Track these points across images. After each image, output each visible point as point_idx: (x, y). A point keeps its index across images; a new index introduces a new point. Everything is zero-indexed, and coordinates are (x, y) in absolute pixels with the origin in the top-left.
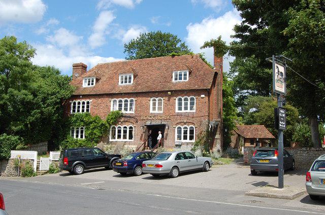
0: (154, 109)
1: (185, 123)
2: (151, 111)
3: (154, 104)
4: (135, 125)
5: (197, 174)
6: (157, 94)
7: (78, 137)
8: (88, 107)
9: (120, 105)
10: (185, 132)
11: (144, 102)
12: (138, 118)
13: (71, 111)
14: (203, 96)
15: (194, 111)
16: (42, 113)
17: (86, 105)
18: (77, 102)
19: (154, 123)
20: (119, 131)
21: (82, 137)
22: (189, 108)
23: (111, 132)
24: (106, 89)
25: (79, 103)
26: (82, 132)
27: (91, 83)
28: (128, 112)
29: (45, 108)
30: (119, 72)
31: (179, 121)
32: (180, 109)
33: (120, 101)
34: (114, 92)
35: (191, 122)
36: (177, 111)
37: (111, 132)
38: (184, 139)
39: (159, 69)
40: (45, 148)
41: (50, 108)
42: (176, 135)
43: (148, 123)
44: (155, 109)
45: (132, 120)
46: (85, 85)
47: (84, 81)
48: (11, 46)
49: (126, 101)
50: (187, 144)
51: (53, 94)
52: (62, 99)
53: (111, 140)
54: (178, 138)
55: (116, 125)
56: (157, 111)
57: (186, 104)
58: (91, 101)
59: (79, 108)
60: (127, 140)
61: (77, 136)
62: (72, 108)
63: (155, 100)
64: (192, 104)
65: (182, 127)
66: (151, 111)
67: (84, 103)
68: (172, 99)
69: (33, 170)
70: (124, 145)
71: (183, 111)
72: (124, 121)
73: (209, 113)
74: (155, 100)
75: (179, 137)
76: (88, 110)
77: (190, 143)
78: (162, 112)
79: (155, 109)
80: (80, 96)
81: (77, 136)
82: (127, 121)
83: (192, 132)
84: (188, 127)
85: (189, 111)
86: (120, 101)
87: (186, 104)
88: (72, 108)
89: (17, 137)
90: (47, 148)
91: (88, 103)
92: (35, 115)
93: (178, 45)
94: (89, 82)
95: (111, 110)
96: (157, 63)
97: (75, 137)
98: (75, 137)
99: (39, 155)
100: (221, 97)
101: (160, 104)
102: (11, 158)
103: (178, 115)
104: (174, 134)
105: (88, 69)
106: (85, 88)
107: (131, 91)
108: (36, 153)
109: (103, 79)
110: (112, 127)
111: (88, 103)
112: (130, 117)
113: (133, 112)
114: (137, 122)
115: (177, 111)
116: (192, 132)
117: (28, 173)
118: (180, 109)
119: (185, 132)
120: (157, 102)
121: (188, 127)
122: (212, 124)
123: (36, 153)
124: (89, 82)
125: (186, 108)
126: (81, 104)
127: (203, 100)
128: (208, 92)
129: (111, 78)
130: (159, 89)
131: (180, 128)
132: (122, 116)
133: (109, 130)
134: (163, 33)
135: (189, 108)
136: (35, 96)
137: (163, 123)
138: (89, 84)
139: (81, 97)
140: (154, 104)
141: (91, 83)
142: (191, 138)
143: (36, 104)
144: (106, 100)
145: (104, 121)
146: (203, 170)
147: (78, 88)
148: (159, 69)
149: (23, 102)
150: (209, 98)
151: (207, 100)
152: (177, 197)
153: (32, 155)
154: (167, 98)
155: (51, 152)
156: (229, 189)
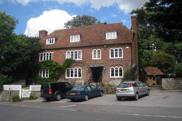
0: (95, 57)
1: (116, 66)
2: (93, 58)
3: (95, 54)
4: (82, 68)
5: (94, 99)
6: (97, 47)
7: (44, 75)
8: (50, 57)
9: (72, 55)
10: (117, 71)
11: (88, 53)
12: (84, 63)
13: (40, 60)
14: (127, 47)
15: (122, 57)
16: (23, 60)
17: (49, 56)
18: (43, 54)
19: (95, 66)
20: (72, 72)
21: (47, 76)
22: (114, 56)
23: (66, 71)
24: (63, 45)
25: (45, 55)
26: (47, 73)
27: (52, 42)
28: (78, 59)
29: (25, 57)
30: (69, 34)
31: (112, 64)
32: (112, 56)
33: (72, 52)
34: (67, 46)
35: (120, 64)
36: (110, 58)
37: (66, 71)
38: (116, 76)
39: (96, 32)
40: (24, 83)
41: (27, 57)
42: (110, 73)
43: (92, 66)
44: (96, 56)
45: (80, 64)
46: (48, 43)
47: (47, 40)
48: (2, 17)
49: (76, 52)
50: (118, 79)
51: (29, 48)
52: (34, 52)
53: (66, 78)
54: (120, 75)
55: (70, 68)
56: (97, 58)
57: (116, 53)
58: (53, 53)
59: (45, 57)
60: (78, 77)
61: (44, 75)
62: (40, 58)
63: (95, 51)
64: (120, 53)
65: (114, 68)
66: (93, 58)
67: (48, 54)
68: (108, 49)
69: (19, 97)
70: (76, 80)
71: (115, 57)
72: (75, 65)
73: (132, 59)
74: (68, 52)
75: (113, 75)
76: (50, 59)
77: (120, 78)
78: (100, 59)
79: (96, 56)
80: (45, 49)
81: (44, 75)
82: (77, 65)
83: (121, 71)
84: (119, 68)
85: (118, 57)
86: (72, 52)
87: (116, 53)
88: (40, 58)
89: (7, 76)
90: (25, 83)
91: (51, 54)
92: (15, 64)
93: (97, 22)
94: (51, 41)
95: (66, 58)
96: (94, 28)
97: (42, 76)
98: (42, 76)
99: (23, 87)
100: (137, 49)
101: (99, 53)
102: (4, 90)
103: (111, 60)
104: (109, 73)
105: (48, 34)
106: (48, 45)
107: (79, 46)
108: (20, 86)
109: (60, 39)
110: (67, 69)
111: (51, 54)
112: (79, 62)
113: (81, 59)
114: (84, 65)
115: (110, 58)
116: (121, 71)
117: (16, 98)
118: (112, 56)
119: (117, 71)
120: (97, 52)
121: (119, 68)
122: (134, 66)
123: (20, 86)
124: (51, 41)
125: (116, 56)
126: (46, 55)
127: (128, 50)
128: (130, 44)
129: (64, 38)
130: (98, 44)
131: (113, 68)
132: (74, 61)
133: (65, 71)
134: (87, 16)
135: (114, 56)
136: (18, 49)
137: (101, 66)
138: (50, 43)
139: (46, 50)
140: (95, 54)
141: (52, 42)
142: (121, 75)
143: (19, 54)
144: (63, 51)
145: (61, 64)
146: (147, 95)
147: (44, 45)
148: (96, 32)
149: (9, 53)
150: (131, 48)
151: (130, 50)
152: (156, 115)
153: (17, 87)
154: (104, 49)
155: (30, 86)
156: (156, 106)
